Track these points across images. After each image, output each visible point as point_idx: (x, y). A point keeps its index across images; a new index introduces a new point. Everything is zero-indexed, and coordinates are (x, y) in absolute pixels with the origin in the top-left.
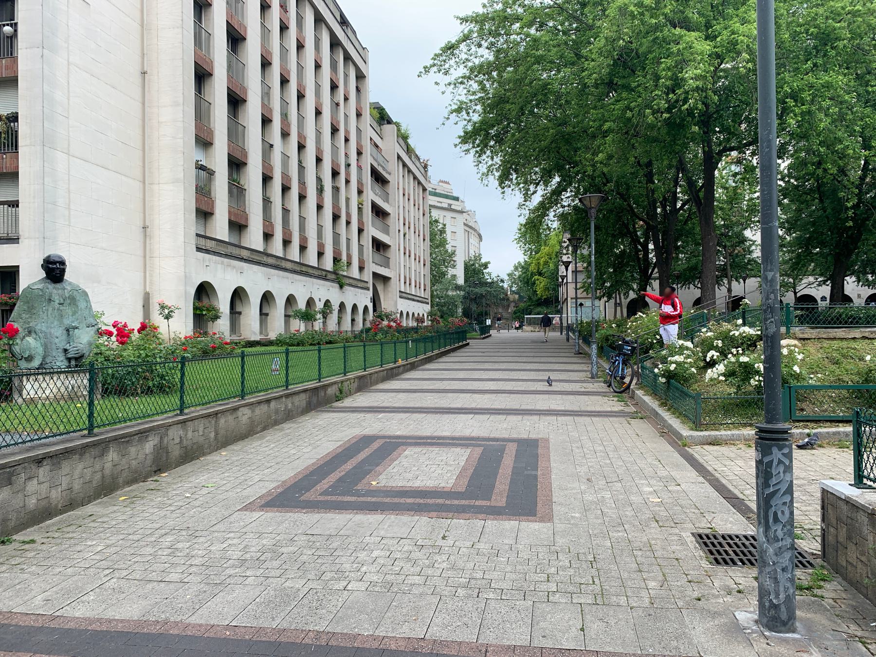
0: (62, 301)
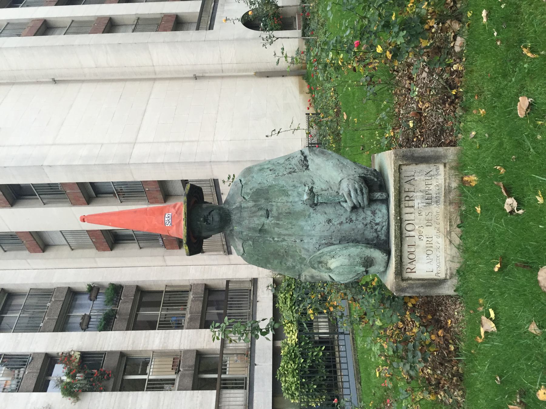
0: (263, 212)
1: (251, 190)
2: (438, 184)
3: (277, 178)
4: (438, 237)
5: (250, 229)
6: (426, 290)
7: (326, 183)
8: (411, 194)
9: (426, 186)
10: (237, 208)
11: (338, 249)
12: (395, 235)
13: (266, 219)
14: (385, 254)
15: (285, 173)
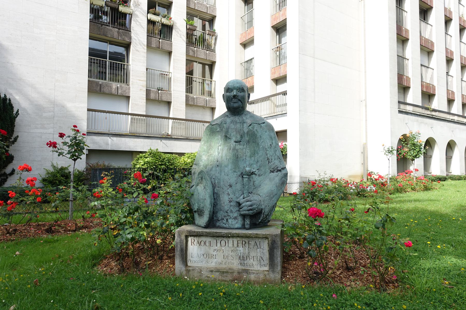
1: (256, 130)
2: (254, 265)
3: (265, 149)
4: (216, 263)
8: (247, 245)
10: (243, 120)
14: (205, 225)
15: (268, 156)
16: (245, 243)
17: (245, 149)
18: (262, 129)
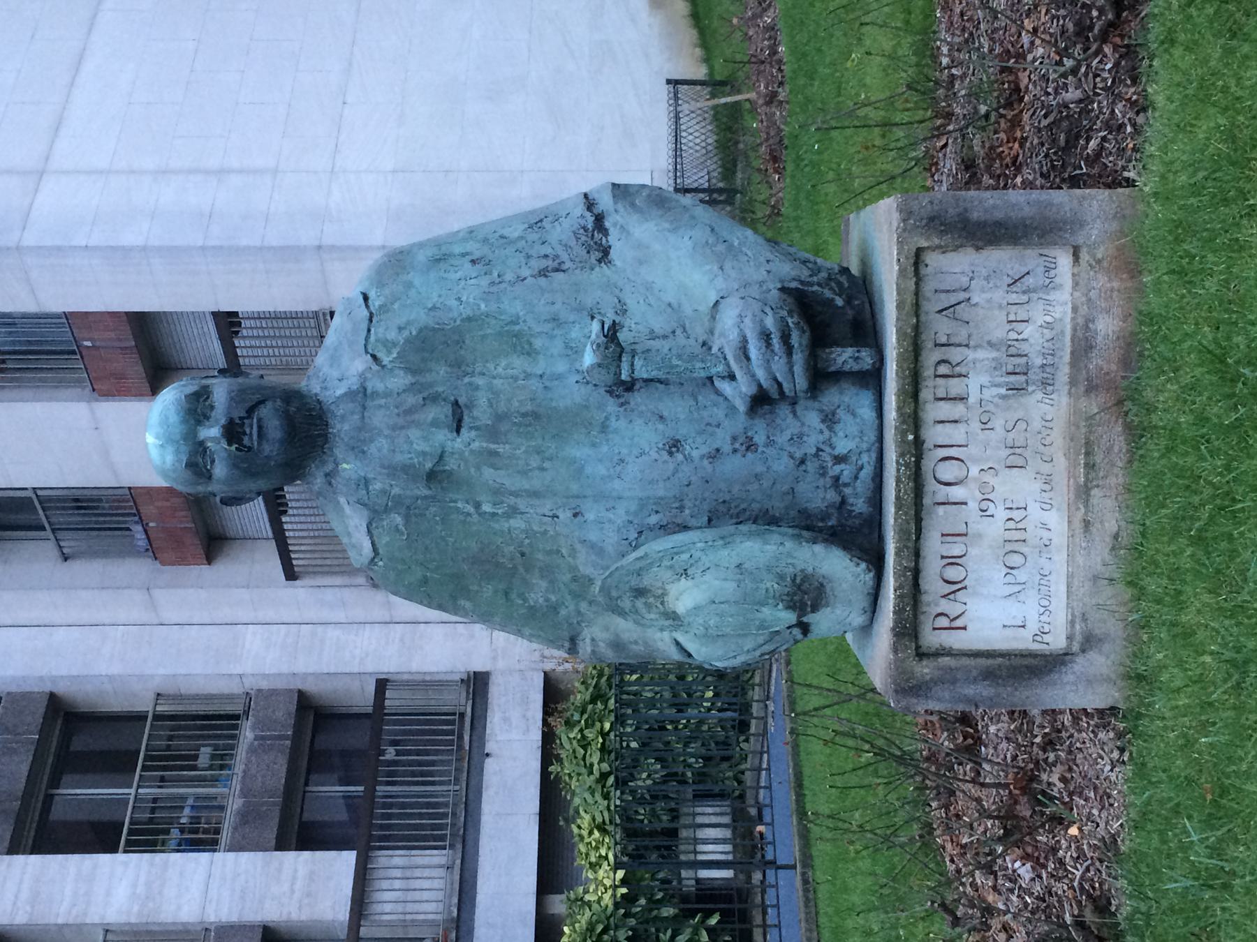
0: (441, 412)
1: (400, 329)
2: (1048, 319)
3: (493, 289)
4: (1046, 506)
5: (393, 470)
6: (1001, 689)
7: (669, 310)
8: (955, 355)
9: (1008, 327)
10: (350, 395)
11: (699, 545)
12: (898, 498)
13: (450, 436)
14: (863, 565)
15: (525, 272)
16: (944, 361)
17: (495, 382)
18: (396, 306)
